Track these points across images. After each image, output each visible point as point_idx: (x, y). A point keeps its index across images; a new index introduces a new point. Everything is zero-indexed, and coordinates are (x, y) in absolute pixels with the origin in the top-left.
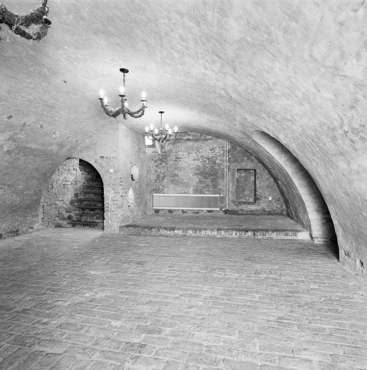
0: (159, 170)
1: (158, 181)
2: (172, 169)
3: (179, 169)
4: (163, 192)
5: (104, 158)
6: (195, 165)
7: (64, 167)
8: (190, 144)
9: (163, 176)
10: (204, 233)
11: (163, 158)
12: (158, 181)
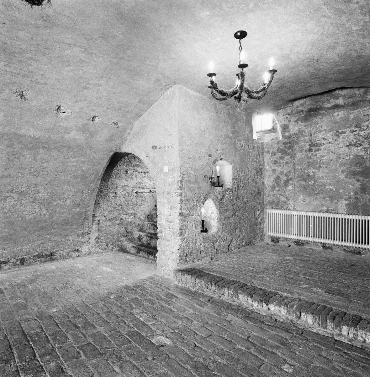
0: (279, 169)
1: (277, 189)
2: (304, 166)
3: (317, 166)
4: (286, 207)
5: (157, 149)
6: (351, 157)
7: (136, 168)
8: (340, 114)
9: (285, 178)
10: (351, 336)
11: (285, 147)
12: (277, 189)
